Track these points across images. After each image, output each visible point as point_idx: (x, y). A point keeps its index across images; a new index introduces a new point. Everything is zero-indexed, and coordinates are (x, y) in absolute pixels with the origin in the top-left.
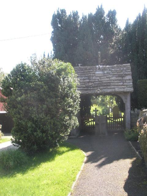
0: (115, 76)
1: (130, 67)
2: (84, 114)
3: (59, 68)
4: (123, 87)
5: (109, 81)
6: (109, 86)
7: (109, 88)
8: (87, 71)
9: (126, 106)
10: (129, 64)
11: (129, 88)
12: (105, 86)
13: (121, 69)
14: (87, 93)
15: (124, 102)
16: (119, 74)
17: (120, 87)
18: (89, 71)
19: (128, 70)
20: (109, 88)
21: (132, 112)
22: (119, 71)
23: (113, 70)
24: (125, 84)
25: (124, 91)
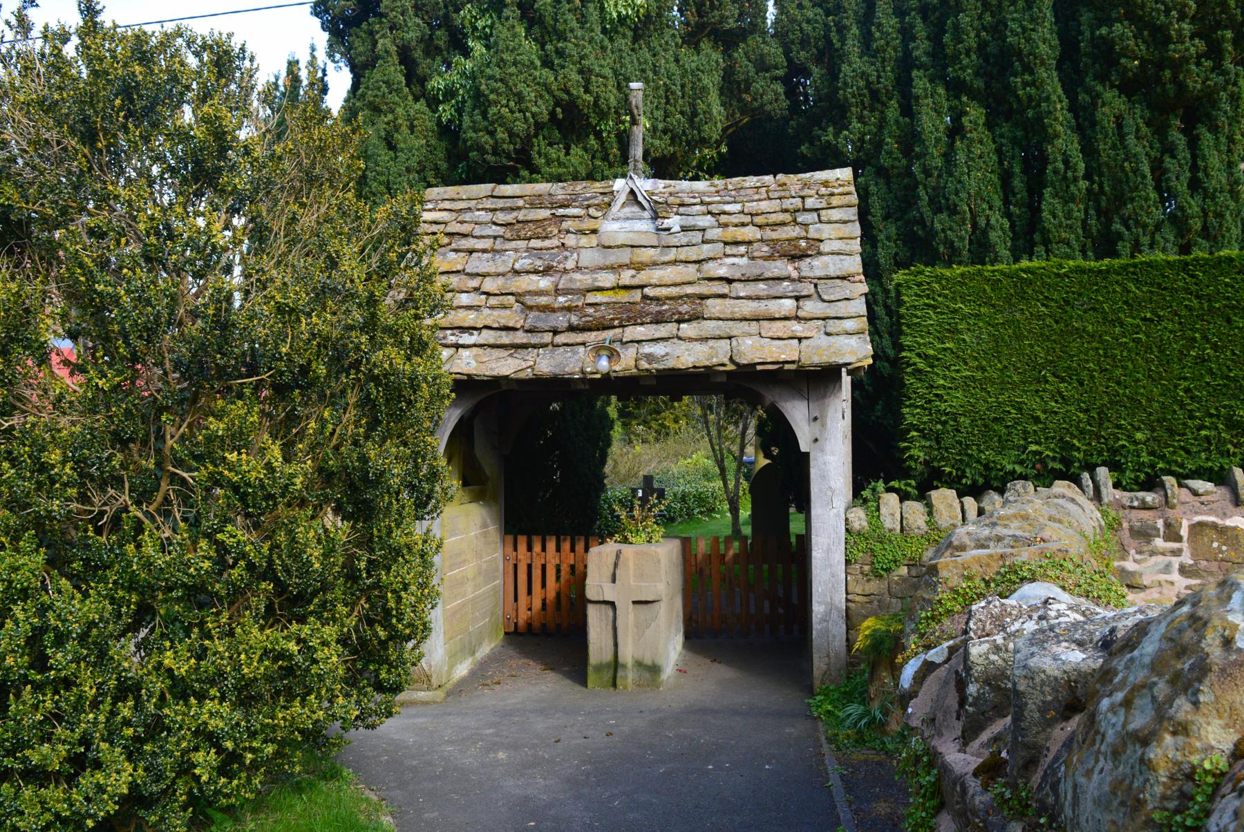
0: (742, 249)
1: (852, 189)
2: (352, 610)
3: (1210, 464)
4: (797, 328)
5: (689, 290)
6: (695, 317)
7: (691, 340)
8: (545, 213)
9: (813, 472)
10: (846, 173)
11: (496, 313)
12: (658, 320)
13: (790, 203)
14: (528, 374)
15: (804, 448)
16: (769, 234)
17: (778, 328)
18: (561, 211)
19: (835, 214)
20: (691, 340)
21: (859, 518)
22: (774, 218)
23: (728, 208)
24: (810, 307)
25: (805, 361)
